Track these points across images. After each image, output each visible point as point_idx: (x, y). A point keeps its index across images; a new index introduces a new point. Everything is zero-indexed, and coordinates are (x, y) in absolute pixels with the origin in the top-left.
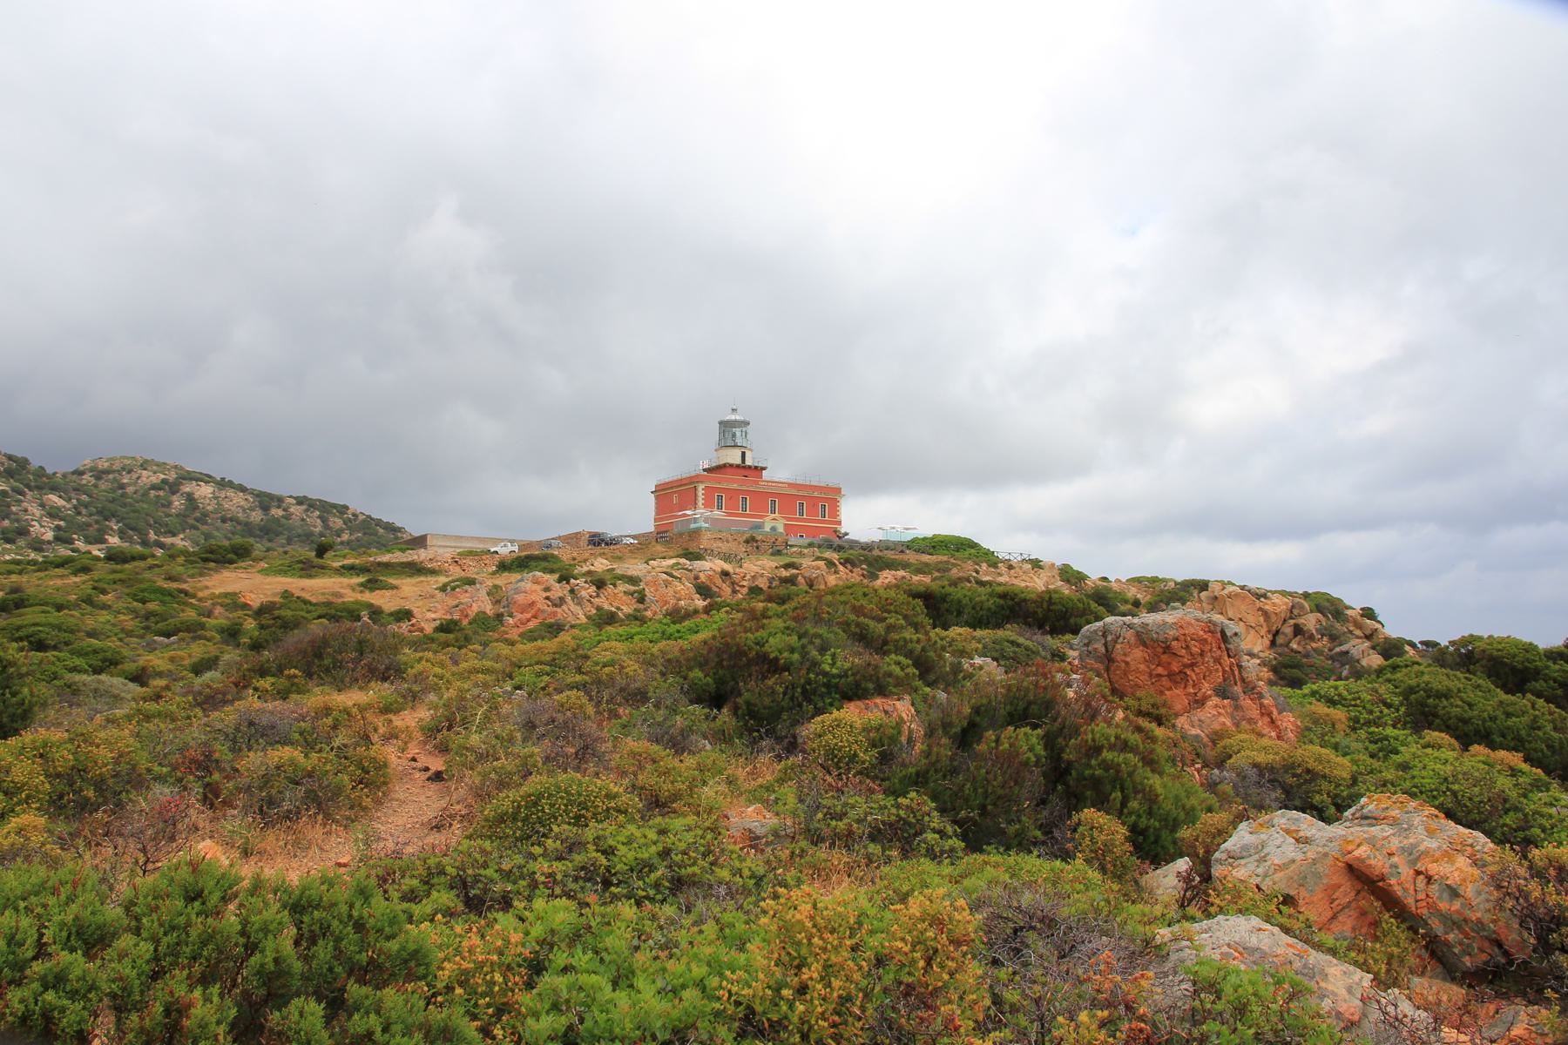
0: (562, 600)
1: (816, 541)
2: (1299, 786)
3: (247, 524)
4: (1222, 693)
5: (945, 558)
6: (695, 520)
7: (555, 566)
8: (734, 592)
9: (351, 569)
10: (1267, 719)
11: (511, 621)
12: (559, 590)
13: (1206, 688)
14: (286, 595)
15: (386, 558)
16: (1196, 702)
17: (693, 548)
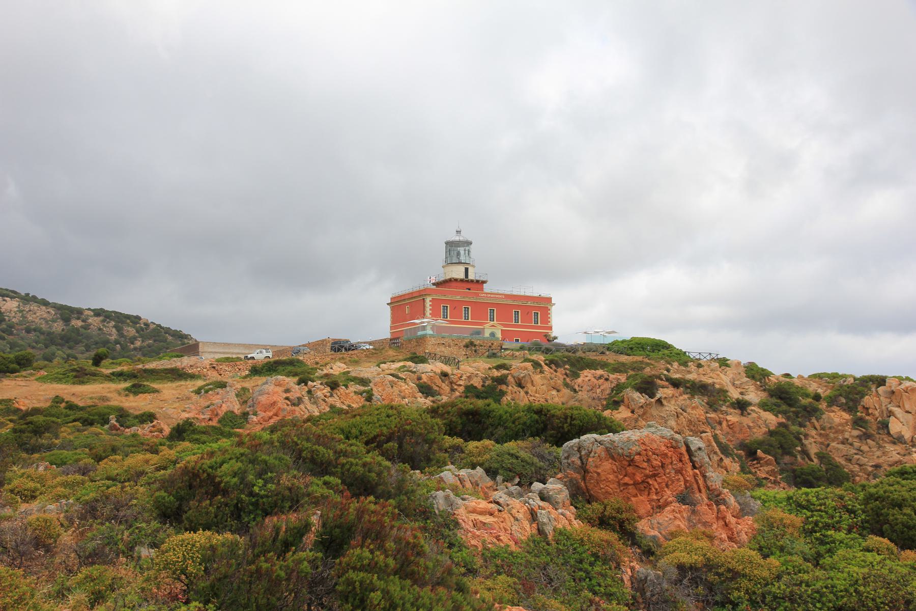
0: (300, 400)
1: (526, 344)
2: (722, 582)
3: (49, 334)
4: (683, 499)
5: (640, 358)
6: (424, 328)
7: (299, 370)
8: (453, 390)
9: (120, 376)
10: (721, 523)
11: (255, 419)
12: (298, 391)
13: (668, 495)
14: (58, 400)
15: (152, 365)
16: (659, 507)
17: (420, 352)
